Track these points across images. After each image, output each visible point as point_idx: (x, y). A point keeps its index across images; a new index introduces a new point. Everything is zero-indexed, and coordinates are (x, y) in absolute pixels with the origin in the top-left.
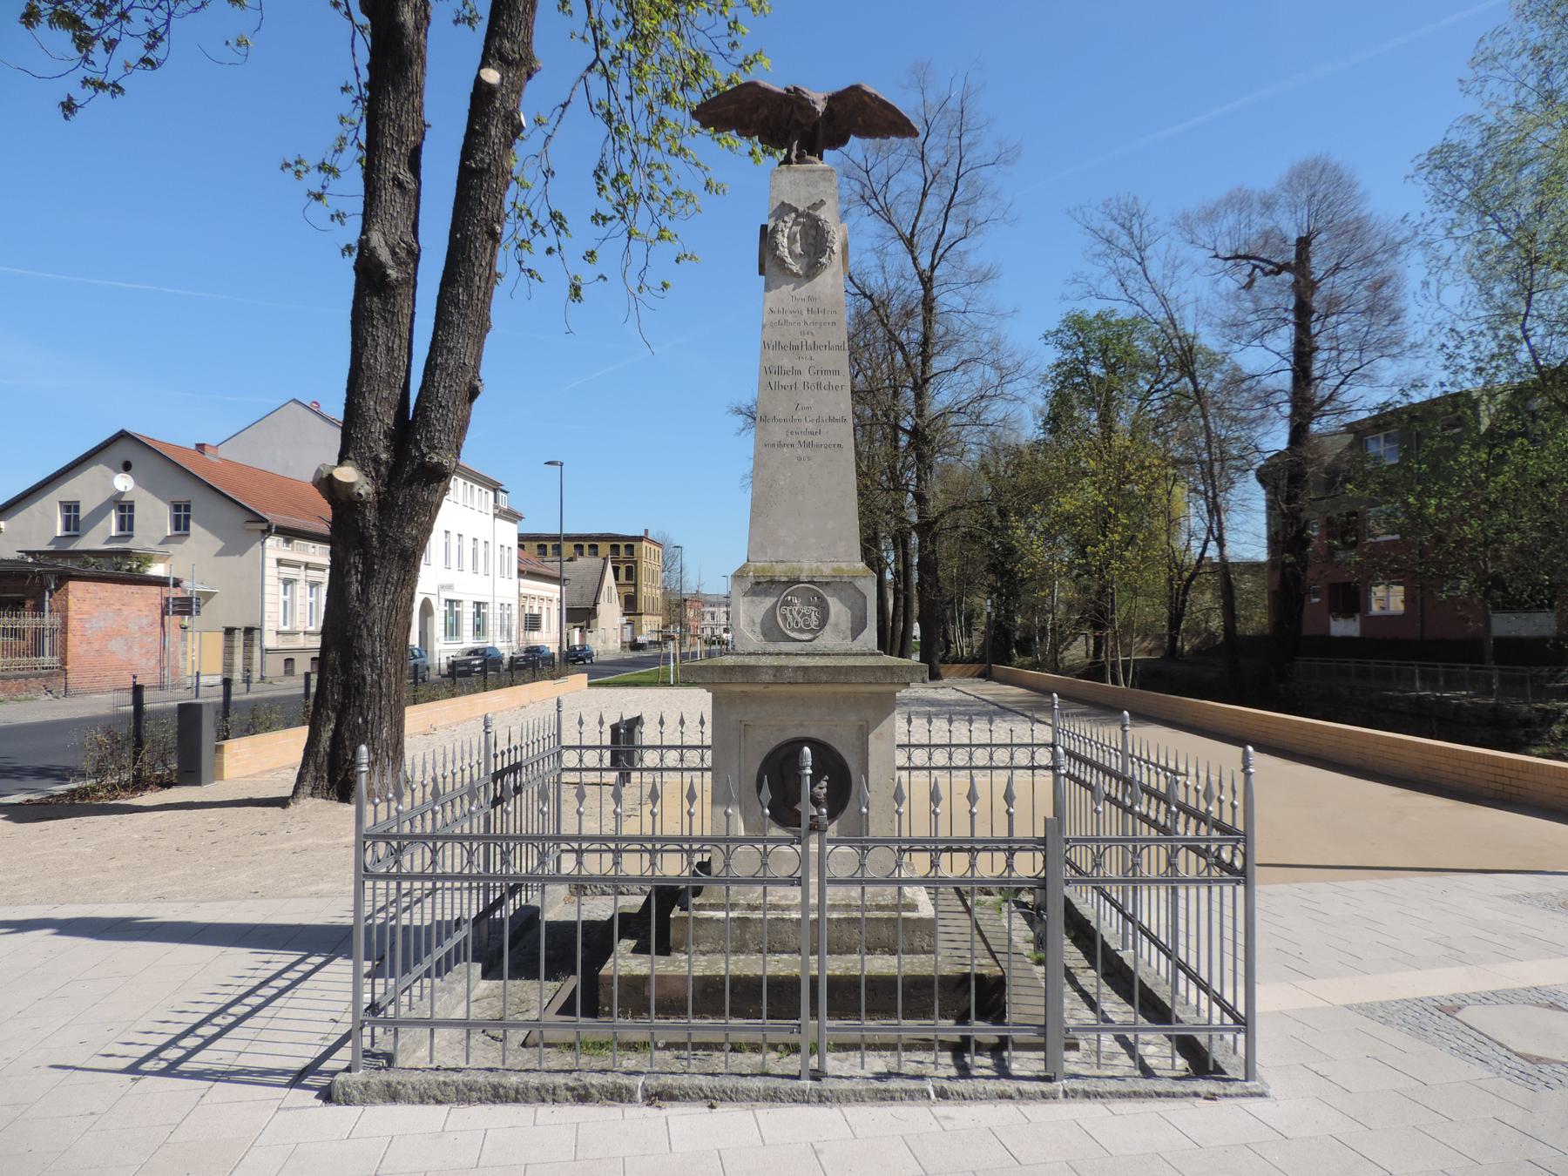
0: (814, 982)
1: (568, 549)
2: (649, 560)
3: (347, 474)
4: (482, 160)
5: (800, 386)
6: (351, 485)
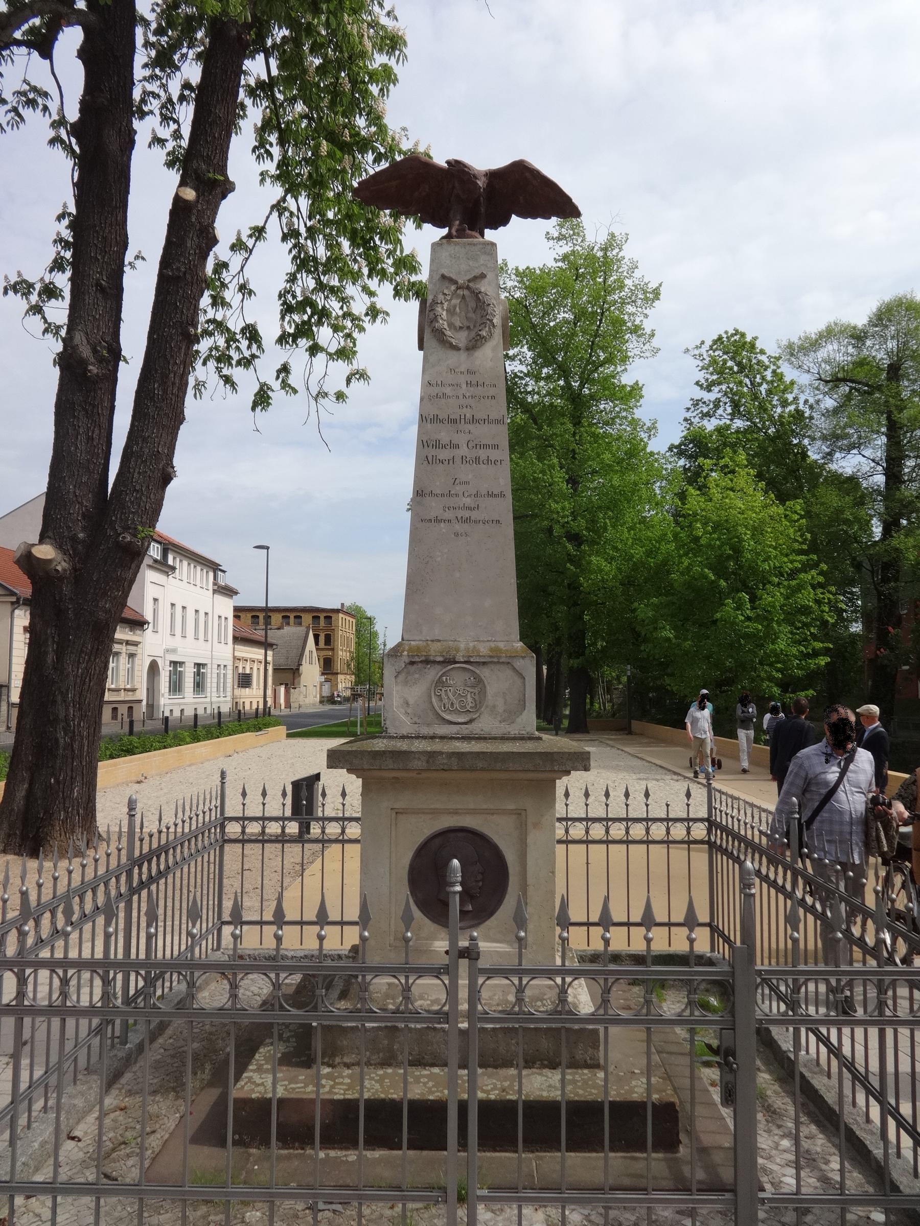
0: (463, 1107)
1: (276, 619)
2: (345, 629)
3: (46, 552)
4: (178, 269)
5: (458, 460)
6: (50, 561)
